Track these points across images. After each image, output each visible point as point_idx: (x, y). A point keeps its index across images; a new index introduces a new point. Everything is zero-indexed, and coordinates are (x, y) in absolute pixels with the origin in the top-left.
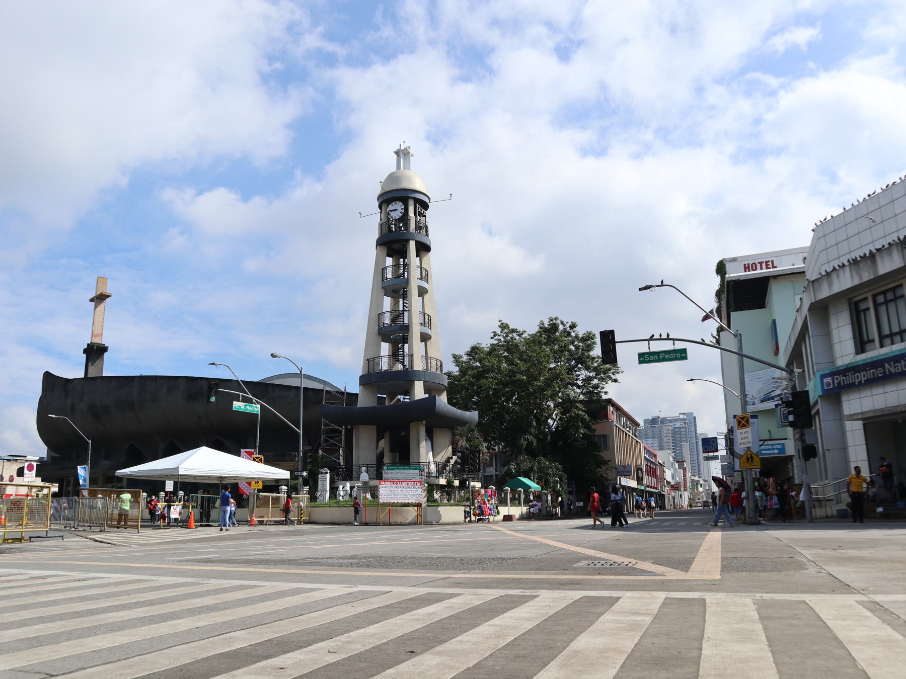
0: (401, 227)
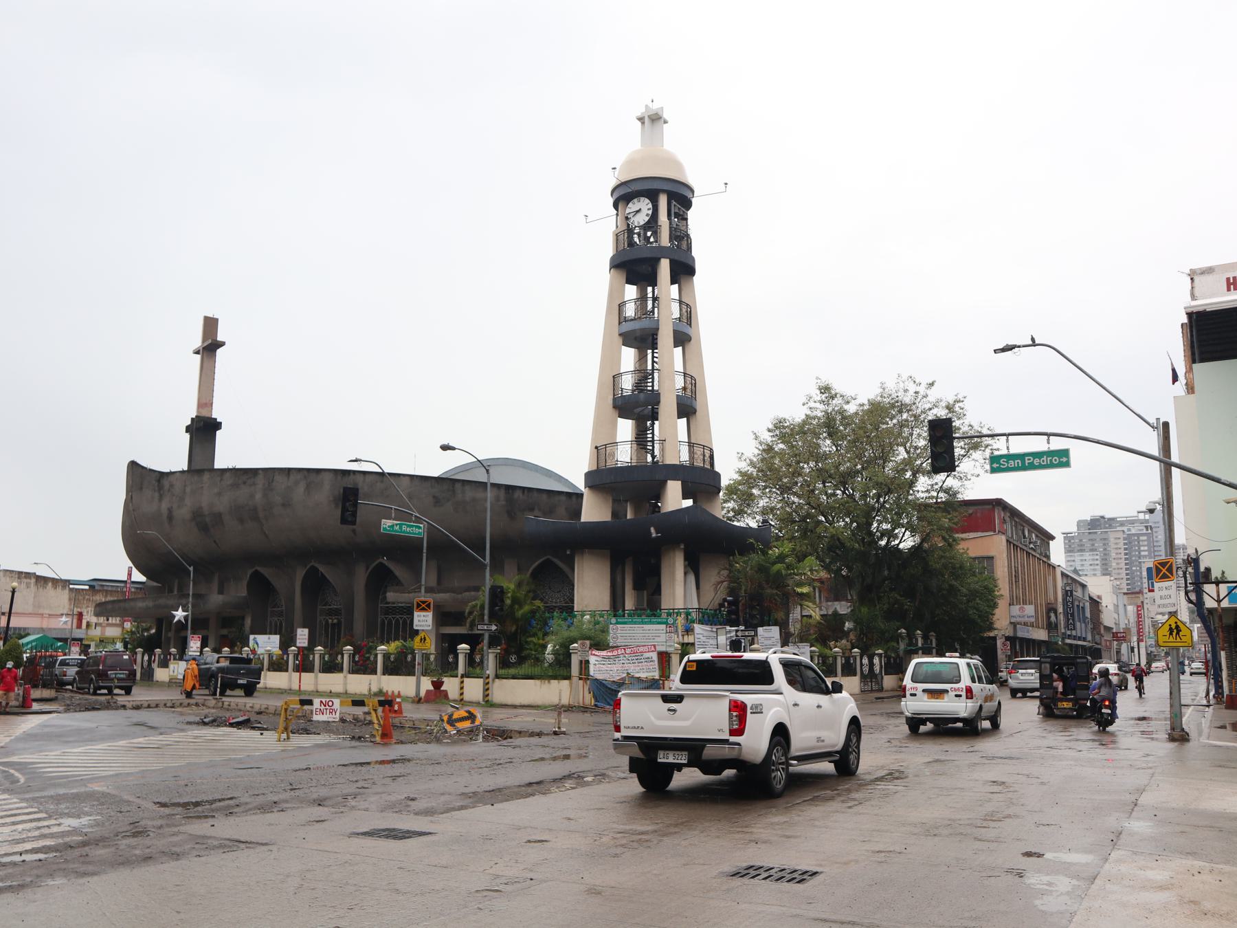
0: (650, 237)
